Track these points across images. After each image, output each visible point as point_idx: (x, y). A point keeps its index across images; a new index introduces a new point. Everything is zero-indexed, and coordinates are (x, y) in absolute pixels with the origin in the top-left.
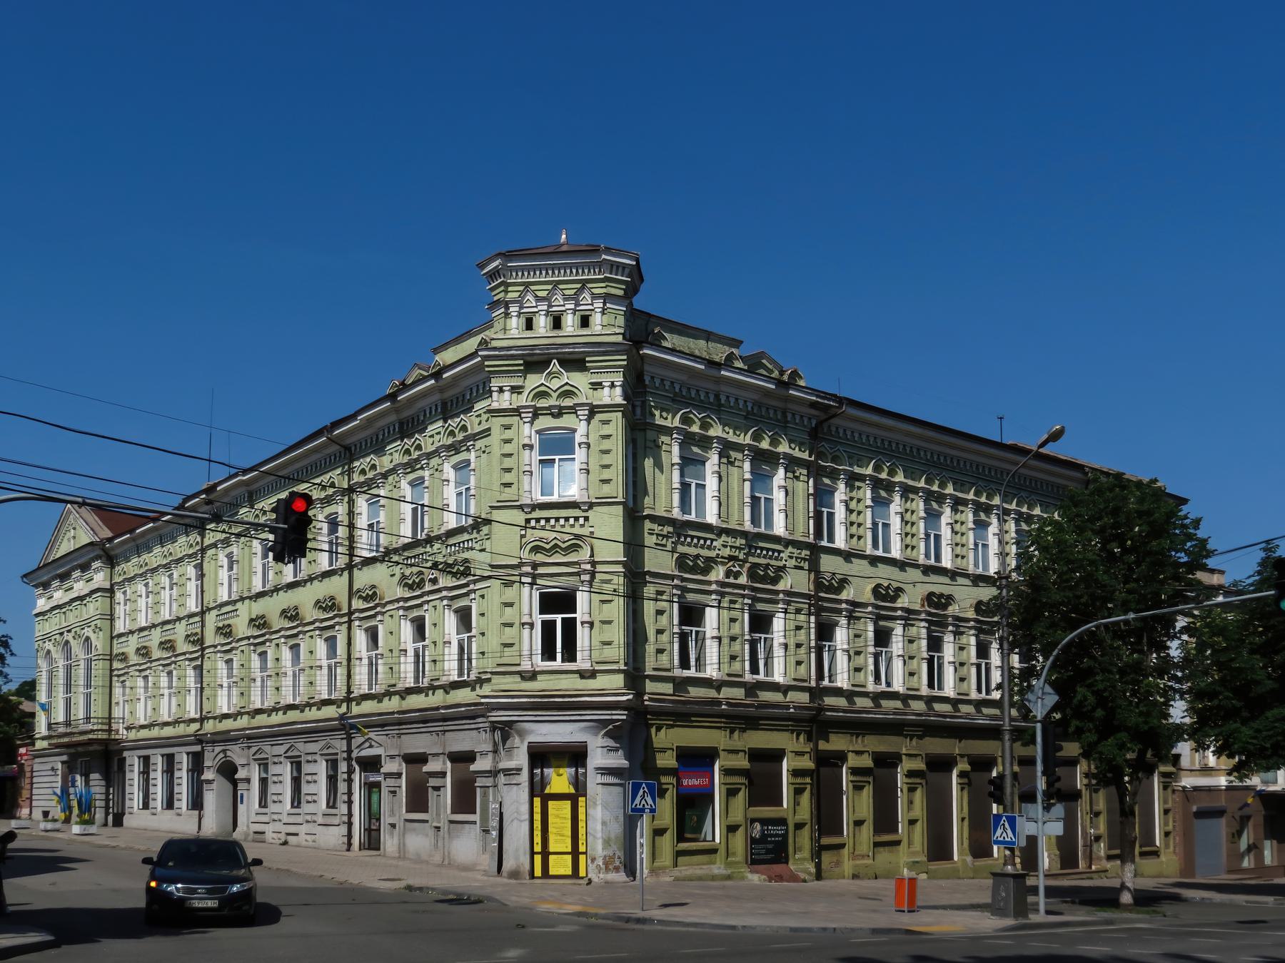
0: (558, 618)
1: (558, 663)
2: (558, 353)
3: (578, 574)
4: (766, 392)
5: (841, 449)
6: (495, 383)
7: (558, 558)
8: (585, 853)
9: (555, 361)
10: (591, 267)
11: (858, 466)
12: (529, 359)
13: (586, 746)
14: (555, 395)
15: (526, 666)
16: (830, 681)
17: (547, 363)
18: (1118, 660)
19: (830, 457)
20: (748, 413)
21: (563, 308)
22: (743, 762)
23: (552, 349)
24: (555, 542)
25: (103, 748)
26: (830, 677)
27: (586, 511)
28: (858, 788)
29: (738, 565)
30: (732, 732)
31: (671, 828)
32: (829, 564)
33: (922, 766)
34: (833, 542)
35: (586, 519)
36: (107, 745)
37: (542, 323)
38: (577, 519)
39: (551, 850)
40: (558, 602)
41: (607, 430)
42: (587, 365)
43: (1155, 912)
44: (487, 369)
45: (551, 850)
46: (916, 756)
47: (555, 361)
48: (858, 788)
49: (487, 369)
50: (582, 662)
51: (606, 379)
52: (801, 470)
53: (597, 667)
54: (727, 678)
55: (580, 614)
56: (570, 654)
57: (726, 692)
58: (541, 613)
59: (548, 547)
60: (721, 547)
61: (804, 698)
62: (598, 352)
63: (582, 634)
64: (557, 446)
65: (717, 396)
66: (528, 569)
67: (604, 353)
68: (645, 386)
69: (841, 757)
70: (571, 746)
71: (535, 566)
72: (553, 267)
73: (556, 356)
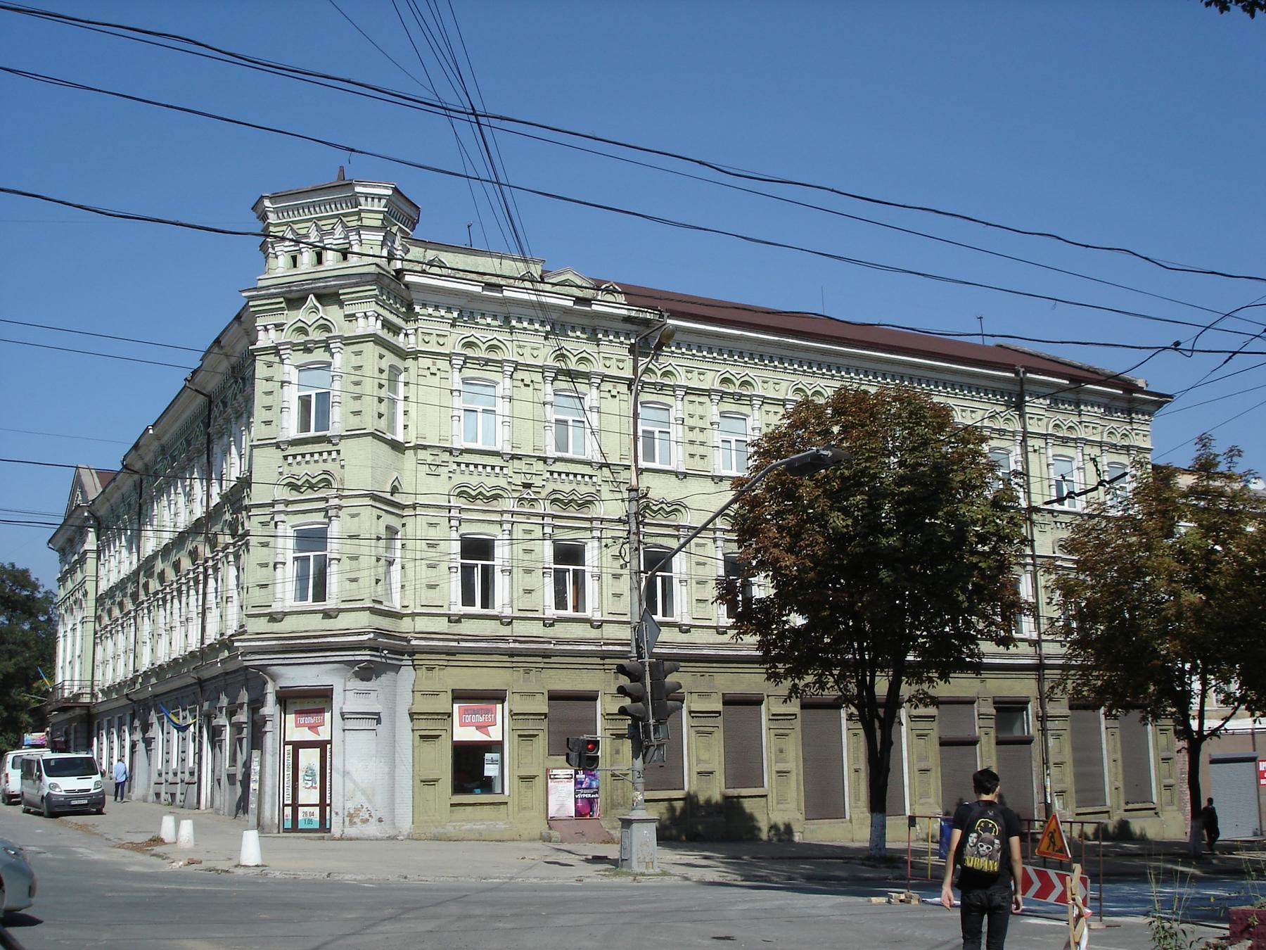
1: (309, 604)
2: (312, 288)
3: (501, 523)
4: (566, 310)
5: (673, 364)
6: (261, 322)
7: (479, 505)
8: (285, 805)
9: (311, 296)
10: (348, 201)
12: (287, 296)
13: (332, 689)
14: (484, 347)
15: (277, 607)
16: (664, 615)
17: (304, 299)
22: (542, 706)
23: (307, 284)
24: (306, 477)
25: (86, 712)
27: (337, 444)
29: (533, 492)
32: (660, 489)
33: (719, 707)
35: (338, 452)
36: (89, 711)
37: (307, 258)
38: (330, 453)
42: (341, 297)
44: (252, 309)
45: (300, 803)
46: (533, 694)
47: (311, 296)
49: (252, 309)
51: (358, 309)
56: (320, 594)
57: (520, 628)
59: (474, 493)
60: (514, 474)
62: (350, 284)
63: (500, 582)
67: (356, 285)
72: (314, 205)
73: (314, 291)
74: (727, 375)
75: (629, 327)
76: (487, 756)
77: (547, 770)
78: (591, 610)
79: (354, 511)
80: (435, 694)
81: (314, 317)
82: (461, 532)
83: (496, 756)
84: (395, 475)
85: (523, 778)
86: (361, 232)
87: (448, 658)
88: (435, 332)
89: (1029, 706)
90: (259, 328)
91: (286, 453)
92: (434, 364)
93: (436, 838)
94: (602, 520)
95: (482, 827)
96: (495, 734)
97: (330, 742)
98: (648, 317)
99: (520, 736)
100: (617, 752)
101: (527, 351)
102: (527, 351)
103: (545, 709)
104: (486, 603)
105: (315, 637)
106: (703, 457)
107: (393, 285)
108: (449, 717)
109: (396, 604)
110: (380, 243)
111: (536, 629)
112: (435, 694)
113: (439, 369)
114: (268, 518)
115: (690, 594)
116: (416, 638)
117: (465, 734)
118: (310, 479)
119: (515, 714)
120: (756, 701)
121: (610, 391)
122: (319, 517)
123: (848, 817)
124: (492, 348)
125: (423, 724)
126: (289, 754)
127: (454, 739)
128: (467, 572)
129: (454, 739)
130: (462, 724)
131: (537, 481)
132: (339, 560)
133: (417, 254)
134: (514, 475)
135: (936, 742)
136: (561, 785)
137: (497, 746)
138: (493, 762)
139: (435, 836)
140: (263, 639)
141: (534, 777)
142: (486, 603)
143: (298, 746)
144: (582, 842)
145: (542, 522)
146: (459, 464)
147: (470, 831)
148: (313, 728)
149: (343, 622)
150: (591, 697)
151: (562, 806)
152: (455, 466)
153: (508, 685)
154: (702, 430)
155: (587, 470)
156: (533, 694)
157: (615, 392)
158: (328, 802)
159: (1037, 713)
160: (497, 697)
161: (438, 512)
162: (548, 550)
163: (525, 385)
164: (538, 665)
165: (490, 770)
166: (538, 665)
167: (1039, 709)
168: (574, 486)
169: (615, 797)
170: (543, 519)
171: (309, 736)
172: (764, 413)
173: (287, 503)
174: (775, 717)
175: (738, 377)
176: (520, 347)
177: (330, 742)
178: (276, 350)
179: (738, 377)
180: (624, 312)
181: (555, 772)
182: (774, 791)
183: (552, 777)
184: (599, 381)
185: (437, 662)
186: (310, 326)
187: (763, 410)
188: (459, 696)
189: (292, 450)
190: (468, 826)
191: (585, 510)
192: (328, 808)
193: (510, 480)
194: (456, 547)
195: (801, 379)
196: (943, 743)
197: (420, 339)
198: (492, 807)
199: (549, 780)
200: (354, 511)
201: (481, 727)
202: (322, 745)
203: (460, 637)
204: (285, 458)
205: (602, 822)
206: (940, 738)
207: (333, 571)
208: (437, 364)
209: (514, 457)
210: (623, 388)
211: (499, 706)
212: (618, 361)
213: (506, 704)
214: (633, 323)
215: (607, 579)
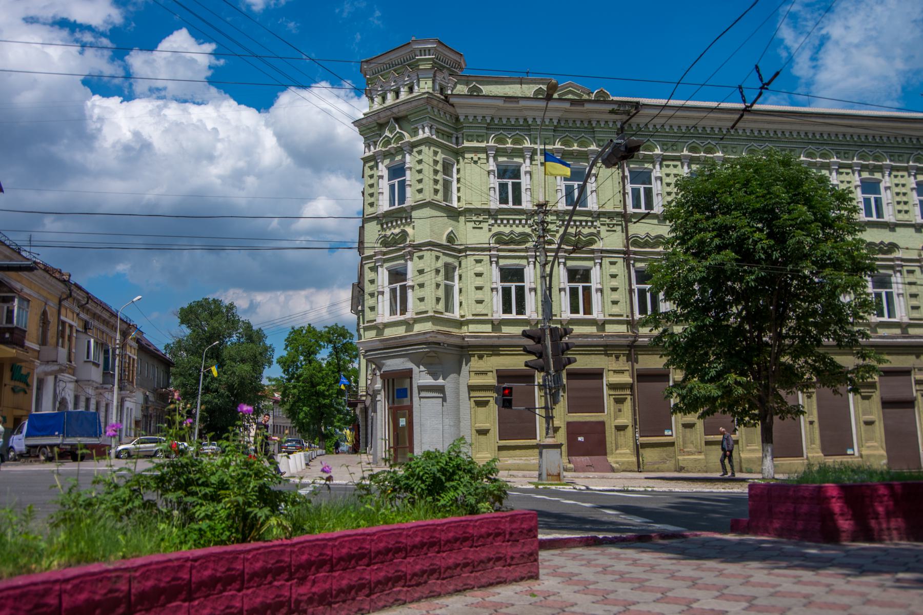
0: (513, 286)
11: (468, 141)
15: (379, 320)
16: (889, 317)
18: (741, 280)
19: (818, 154)
20: (488, 124)
22: (491, 380)
28: (619, 401)
34: (520, 204)
37: (390, 97)
40: (512, 274)
43: (617, 555)
48: (619, 401)
52: (479, 155)
55: (594, 284)
58: (637, 284)
61: (622, 329)
63: (596, 298)
65: (525, 120)
68: (462, 123)
78: (597, 314)
80: (484, 373)
84: (450, 229)
86: (420, 76)
88: (475, 134)
100: (620, 411)
104: (588, 310)
106: (906, 212)
110: (366, 245)
112: (484, 373)
114: (372, 265)
115: (906, 303)
122: (403, 262)
123: (805, 457)
149: (418, 328)
154: (904, 194)
162: (496, 274)
173: (385, 254)
174: (612, 387)
175: (703, 145)
179: (703, 145)
182: (744, 437)
187: (892, 176)
207: (410, 292)
214: (616, 113)
215: (607, 291)
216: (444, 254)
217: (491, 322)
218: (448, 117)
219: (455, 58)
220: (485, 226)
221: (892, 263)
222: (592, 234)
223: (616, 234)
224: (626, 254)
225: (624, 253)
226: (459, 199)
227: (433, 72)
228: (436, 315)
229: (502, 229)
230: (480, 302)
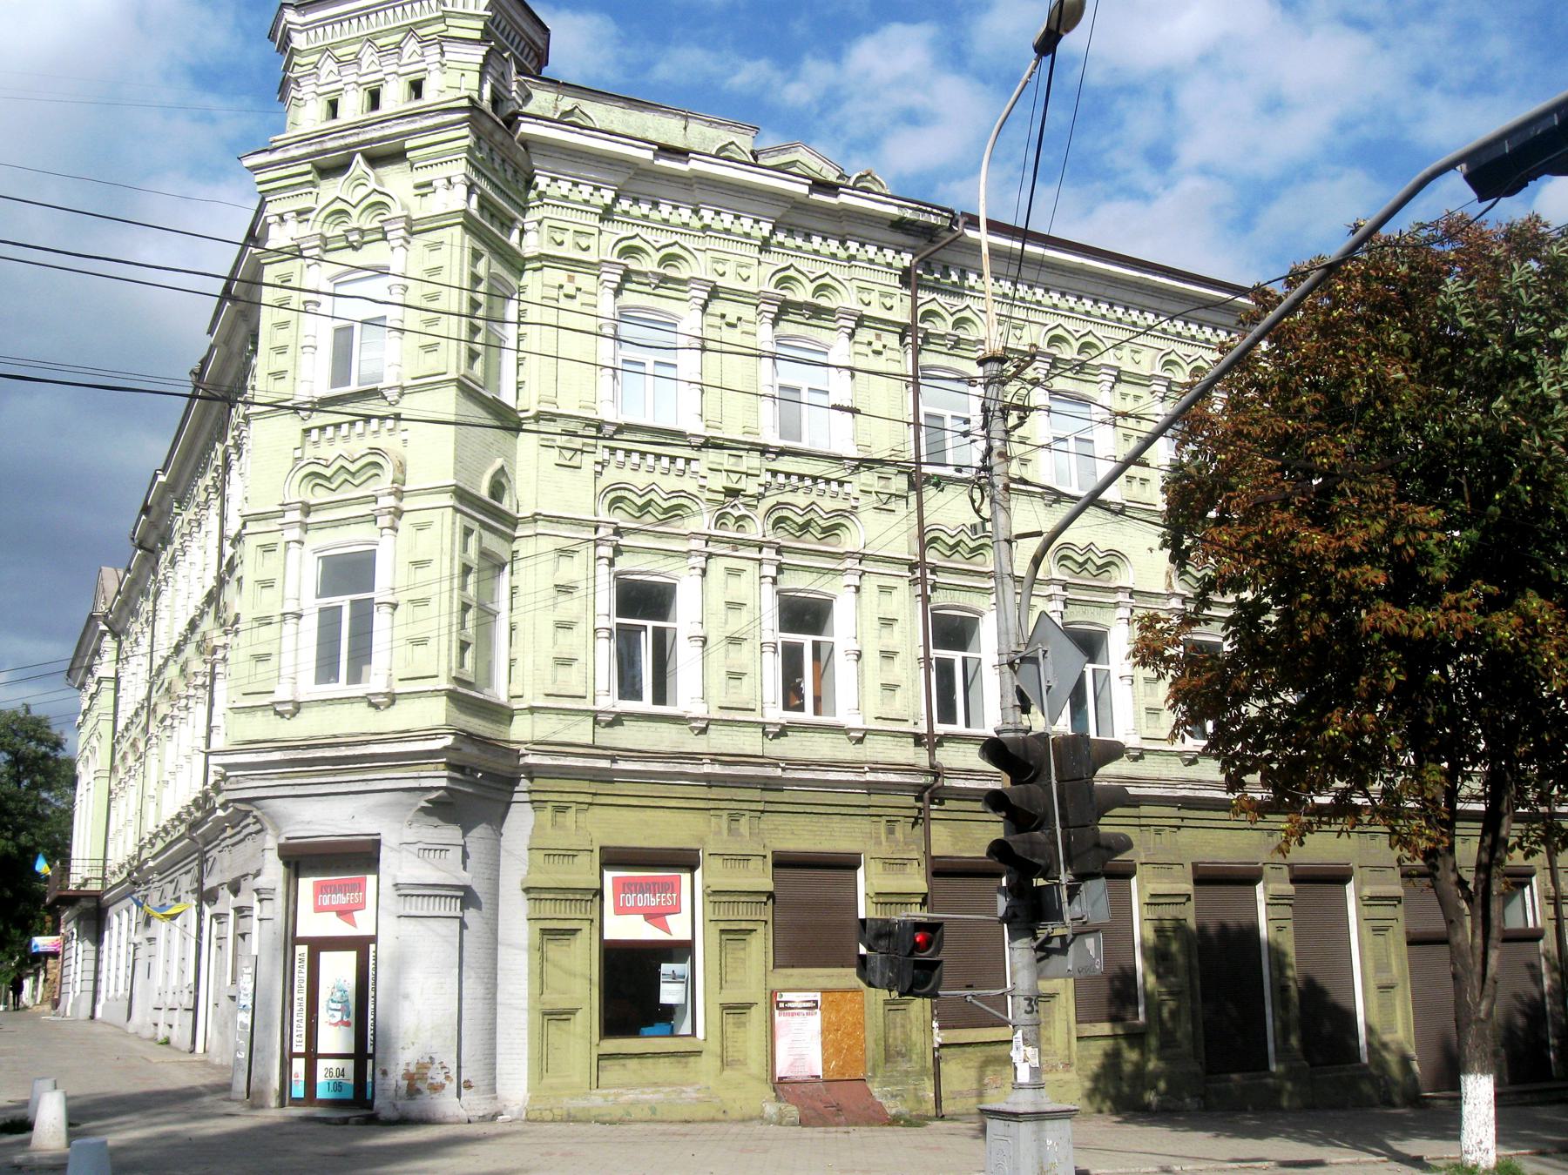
9: (358, 157)
15: (283, 693)
21: (379, 76)
22: (763, 880)
24: (340, 462)
26: (817, 700)
30: (734, 817)
31: (586, 1008)
33: (1187, 887)
39: (320, 1051)
41: (436, 259)
45: (320, 1051)
46: (746, 858)
50: (376, 680)
51: (437, 174)
53: (399, 688)
54: (717, 714)
55: (380, 593)
57: (722, 740)
60: (712, 472)
61: (908, 753)
64: (1293, 549)
66: (296, 516)
69: (1338, 877)
70: (952, 863)
71: (307, 509)
74: (1059, 331)
75: (900, 238)
76: (666, 968)
77: (773, 993)
79: (422, 517)
80: (570, 854)
81: (362, 192)
82: (617, 568)
83: (681, 968)
84: (499, 462)
85: (728, 1008)
87: (594, 788)
88: (573, 227)
89: (1534, 880)
90: (269, 220)
91: (309, 424)
92: (571, 279)
93: (570, 1118)
94: (862, 558)
95: (656, 1096)
96: (678, 928)
97: (373, 939)
98: (933, 221)
99: (722, 931)
101: (730, 268)
102: (730, 268)
103: (768, 886)
104: (660, 697)
105: (347, 744)
107: (499, 137)
108: (595, 896)
109: (500, 692)
110: (477, 67)
111: (749, 742)
112: (570, 854)
113: (579, 289)
116: (536, 752)
117: (626, 927)
118: (349, 478)
119: (715, 892)
120: (1338, 877)
121: (870, 344)
124: (669, 259)
125: (548, 909)
126: (301, 961)
127: (606, 937)
128: (626, 642)
129: (606, 937)
130: (620, 910)
131: (751, 487)
132: (395, 606)
133: (543, 104)
134: (709, 474)
135: (1403, 940)
136: (797, 1019)
137: (681, 951)
138: (675, 978)
139: (569, 1115)
140: (258, 751)
141: (748, 1006)
142: (660, 697)
143: (319, 945)
144: (838, 1125)
145: (759, 556)
146: (613, 450)
147: (633, 1104)
148: (345, 913)
150: (847, 864)
151: (801, 1057)
152: (606, 454)
153: (701, 840)
155: (835, 472)
156: (746, 858)
157: (877, 346)
158: (370, 1050)
159: (1547, 890)
160: (686, 861)
161: (576, 532)
163: (729, 325)
164: (754, 806)
165: (670, 994)
166: (754, 806)
167: (1550, 885)
168: (813, 497)
169: (891, 1040)
170: (760, 551)
171: (332, 926)
172: (1118, 397)
176: (717, 261)
177: (373, 939)
178: (296, 253)
179: (1077, 335)
180: (893, 210)
181: (787, 996)
183: (781, 1005)
184: (852, 325)
185: (573, 797)
186: (354, 207)
188: (614, 858)
189: (319, 419)
190: (631, 1096)
191: (832, 540)
192: (370, 1062)
193: (702, 482)
194: (606, 599)
195: (1174, 346)
196: (1412, 942)
197: (546, 237)
198: (673, 1059)
199: (777, 1012)
200: (422, 517)
201: (655, 916)
202: (362, 946)
203: (615, 753)
204: (307, 431)
205: (869, 1086)
206: (1408, 933)
207: (381, 619)
208: (576, 280)
209: (710, 444)
210: (892, 340)
211: (685, 877)
212: (883, 294)
213: (698, 873)
215: (872, 658)
216: (483, 525)
217: (595, 716)
218: (510, 173)
219: (531, 33)
220: (588, 461)
221: (605, 764)
222: (840, 513)
223: (892, 518)
224: (917, 567)
225: (912, 567)
226: (519, 386)
227: (483, 50)
228: (460, 690)
229: (626, 476)
230: (565, 662)
